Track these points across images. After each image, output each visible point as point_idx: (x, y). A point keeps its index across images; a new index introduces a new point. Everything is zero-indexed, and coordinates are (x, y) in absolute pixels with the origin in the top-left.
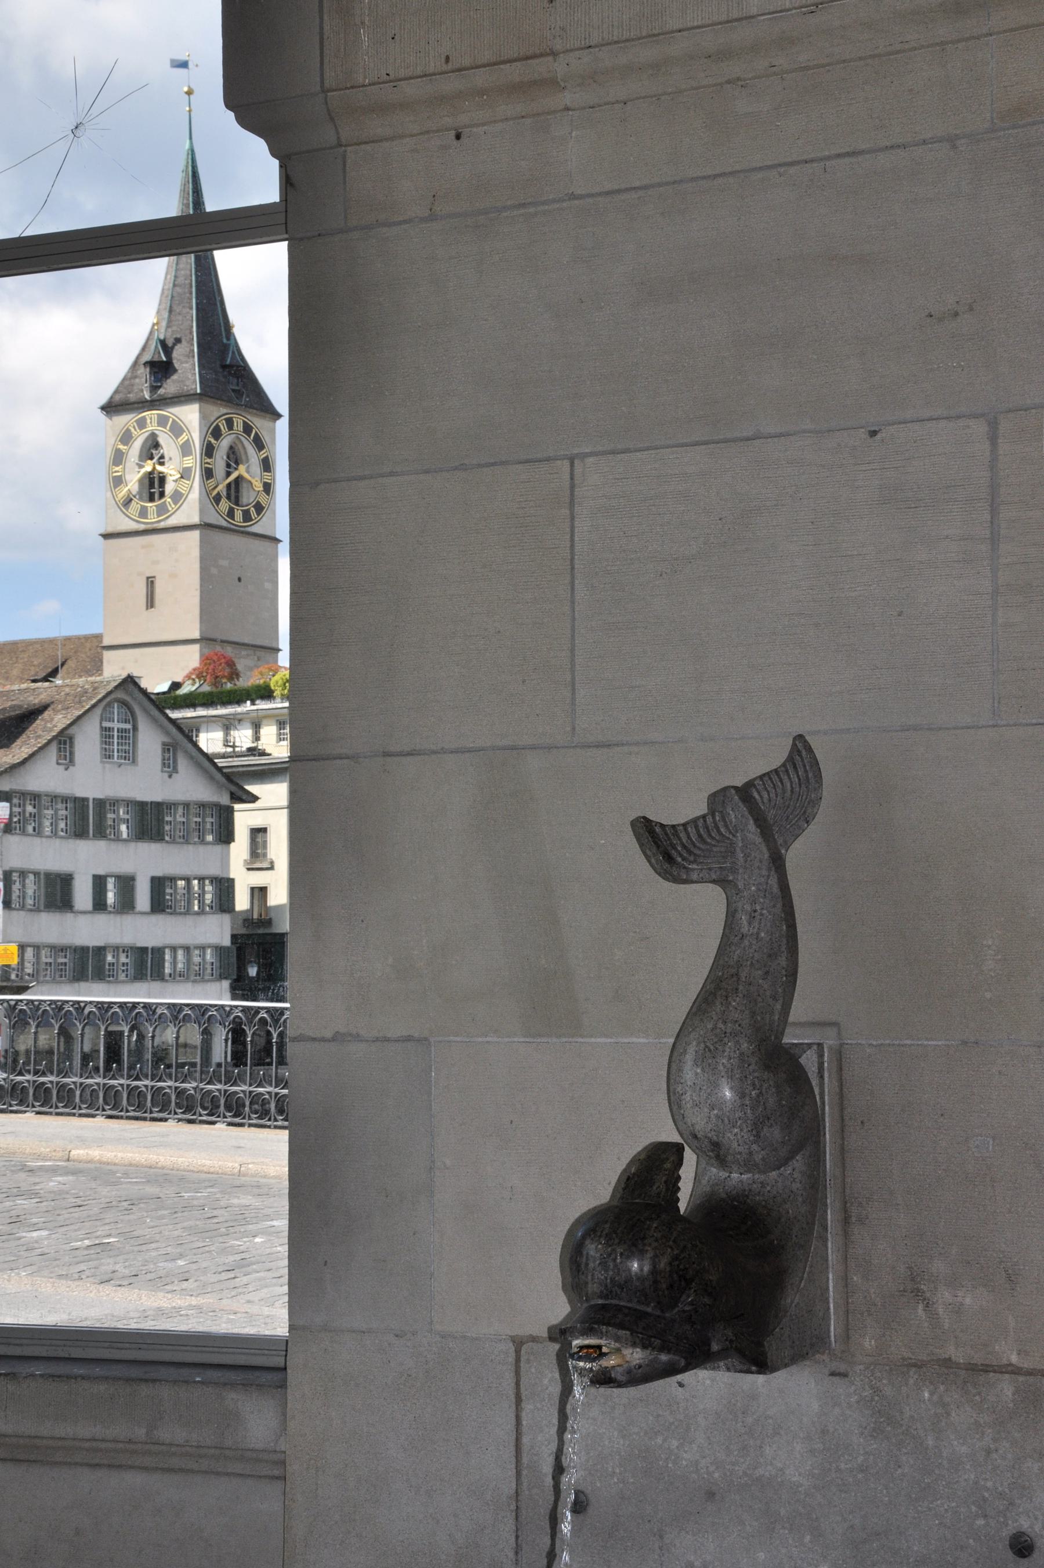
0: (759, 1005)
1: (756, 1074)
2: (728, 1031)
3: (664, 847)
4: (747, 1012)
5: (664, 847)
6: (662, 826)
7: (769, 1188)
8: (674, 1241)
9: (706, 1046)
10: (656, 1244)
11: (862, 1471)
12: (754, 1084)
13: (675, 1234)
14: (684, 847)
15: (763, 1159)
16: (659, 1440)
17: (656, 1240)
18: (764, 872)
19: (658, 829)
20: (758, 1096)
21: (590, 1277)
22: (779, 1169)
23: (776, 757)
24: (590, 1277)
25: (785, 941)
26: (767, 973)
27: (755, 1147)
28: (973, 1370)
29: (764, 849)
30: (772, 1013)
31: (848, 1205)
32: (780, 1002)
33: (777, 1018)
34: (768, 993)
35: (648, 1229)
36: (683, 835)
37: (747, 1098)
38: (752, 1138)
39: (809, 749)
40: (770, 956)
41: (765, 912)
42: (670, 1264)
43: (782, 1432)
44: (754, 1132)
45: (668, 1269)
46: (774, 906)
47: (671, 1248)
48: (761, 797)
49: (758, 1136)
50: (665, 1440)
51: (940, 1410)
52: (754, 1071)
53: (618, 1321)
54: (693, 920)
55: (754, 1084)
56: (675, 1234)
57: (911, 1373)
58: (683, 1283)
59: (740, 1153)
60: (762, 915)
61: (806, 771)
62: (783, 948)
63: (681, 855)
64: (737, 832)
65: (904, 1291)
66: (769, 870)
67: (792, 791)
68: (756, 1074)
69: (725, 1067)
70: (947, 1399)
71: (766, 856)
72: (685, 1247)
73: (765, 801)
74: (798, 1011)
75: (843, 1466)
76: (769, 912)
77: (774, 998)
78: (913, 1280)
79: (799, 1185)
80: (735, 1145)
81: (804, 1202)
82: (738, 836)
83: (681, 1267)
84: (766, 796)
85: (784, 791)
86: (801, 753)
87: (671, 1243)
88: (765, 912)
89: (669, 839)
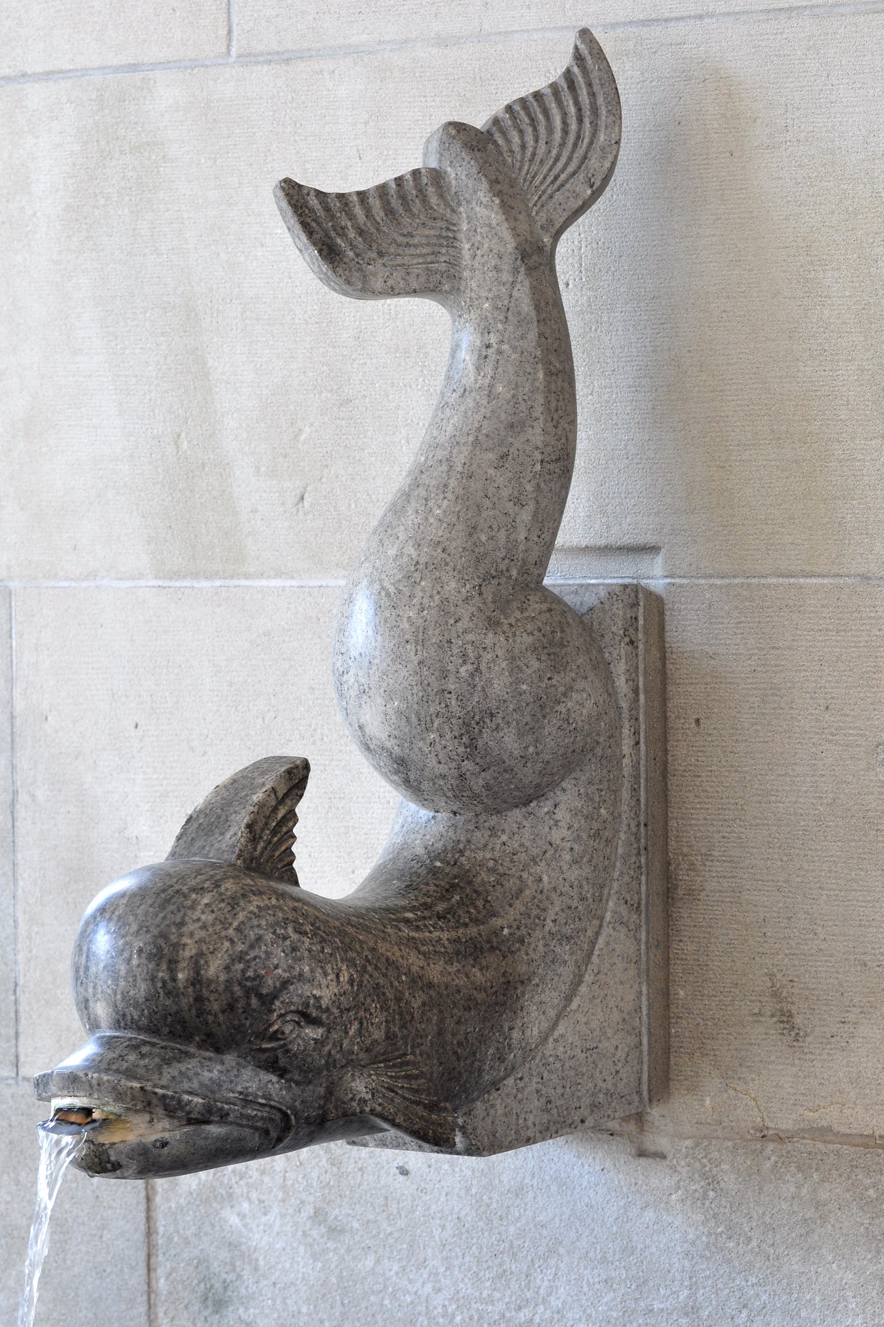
0: (484, 514)
1: (470, 637)
2: (423, 560)
3: (346, 235)
4: (460, 527)
5: (346, 235)
6: (319, 193)
7: (504, 838)
8: (238, 930)
9: (383, 588)
10: (203, 934)
11: (687, 1314)
12: (464, 655)
13: (241, 916)
14: (361, 232)
15: (487, 787)
16: (370, 1262)
17: (204, 927)
18: (506, 277)
19: (313, 202)
20: (472, 675)
21: (90, 990)
22: (526, 804)
23: (563, 61)
24: (90, 990)
25: (540, 399)
26: (504, 457)
27: (468, 765)
28: (866, 1146)
29: (507, 235)
30: (513, 527)
31: (672, 868)
32: (531, 506)
33: (522, 537)
34: (505, 493)
35: (192, 908)
36: (358, 210)
37: (452, 678)
38: (461, 749)
39: (599, 55)
40: (512, 426)
41: (505, 347)
42: (227, 968)
43: (562, 1250)
44: (465, 739)
45: (223, 977)
46: (523, 337)
47: (232, 941)
48: (508, 141)
49: (472, 745)
50: (378, 1261)
51: (810, 1213)
52: (465, 632)
53: (125, 1065)
54: (414, 361)
55: (464, 655)
56: (241, 916)
57: (768, 1151)
58: (254, 1002)
59: (443, 777)
60: (500, 352)
61: (592, 95)
62: (538, 411)
63: (353, 247)
64: (459, 204)
65: (760, 1014)
66: (515, 271)
67: (565, 131)
68: (470, 637)
69: (412, 624)
70: (824, 1196)
71: (511, 245)
72: (259, 939)
73: (516, 148)
74: (576, 524)
75: (657, 1306)
76: (514, 348)
77: (519, 502)
78: (775, 995)
79: (565, 832)
80: (432, 762)
81: (575, 862)
82: (480, 211)
83: (250, 974)
84: (516, 140)
85: (550, 130)
86: (589, 56)
87: (231, 932)
88: (505, 347)
89: (333, 217)
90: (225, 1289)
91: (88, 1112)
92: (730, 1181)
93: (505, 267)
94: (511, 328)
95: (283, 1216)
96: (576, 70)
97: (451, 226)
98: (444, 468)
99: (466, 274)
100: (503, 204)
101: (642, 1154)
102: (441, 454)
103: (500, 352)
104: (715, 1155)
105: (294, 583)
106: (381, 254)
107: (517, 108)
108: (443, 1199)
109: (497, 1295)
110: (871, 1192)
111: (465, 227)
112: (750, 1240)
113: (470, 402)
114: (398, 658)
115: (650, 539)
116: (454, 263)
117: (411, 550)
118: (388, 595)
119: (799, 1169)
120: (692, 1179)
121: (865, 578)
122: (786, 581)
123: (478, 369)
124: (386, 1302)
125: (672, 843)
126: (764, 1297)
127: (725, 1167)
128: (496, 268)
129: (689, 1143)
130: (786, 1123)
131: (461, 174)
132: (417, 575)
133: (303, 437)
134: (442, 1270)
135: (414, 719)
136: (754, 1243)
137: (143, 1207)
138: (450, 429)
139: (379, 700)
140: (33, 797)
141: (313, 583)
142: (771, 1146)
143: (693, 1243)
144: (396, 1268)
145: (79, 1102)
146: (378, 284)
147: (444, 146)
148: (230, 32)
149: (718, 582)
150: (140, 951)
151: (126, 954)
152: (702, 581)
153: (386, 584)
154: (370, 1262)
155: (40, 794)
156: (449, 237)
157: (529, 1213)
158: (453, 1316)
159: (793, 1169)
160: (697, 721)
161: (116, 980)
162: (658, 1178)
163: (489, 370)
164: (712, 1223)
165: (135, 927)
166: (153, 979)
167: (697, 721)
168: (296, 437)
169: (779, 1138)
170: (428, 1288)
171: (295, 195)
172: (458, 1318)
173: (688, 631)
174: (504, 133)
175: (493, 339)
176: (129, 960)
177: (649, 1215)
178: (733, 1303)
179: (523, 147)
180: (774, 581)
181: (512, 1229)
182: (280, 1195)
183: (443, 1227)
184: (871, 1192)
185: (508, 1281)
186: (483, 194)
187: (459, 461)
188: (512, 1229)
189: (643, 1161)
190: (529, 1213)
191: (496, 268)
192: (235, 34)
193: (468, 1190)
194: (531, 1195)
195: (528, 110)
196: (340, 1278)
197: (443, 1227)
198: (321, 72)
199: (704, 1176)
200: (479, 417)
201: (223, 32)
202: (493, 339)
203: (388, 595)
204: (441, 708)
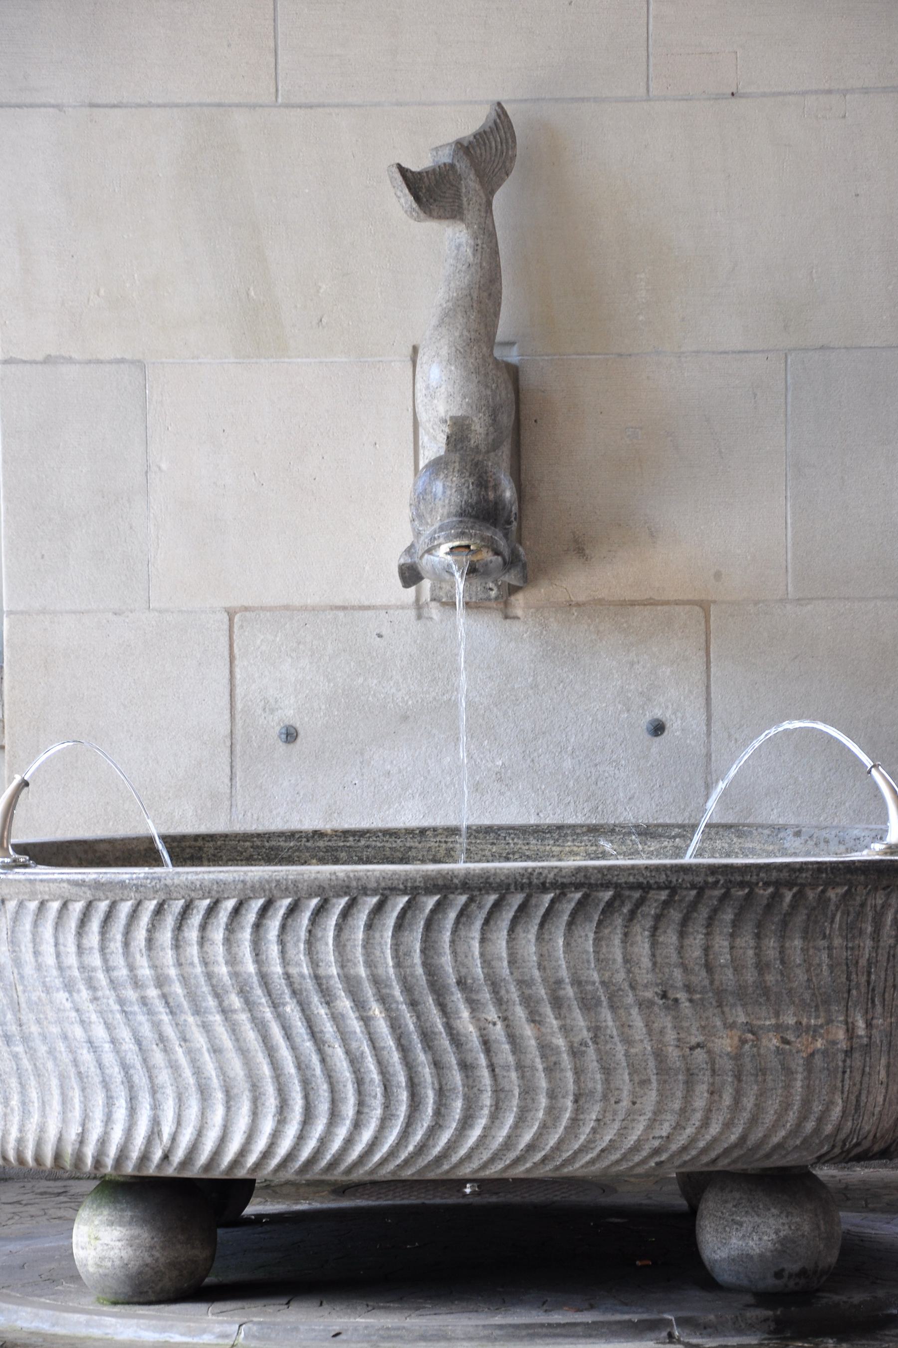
5: (430, 191)
16: (361, 680)
50: (365, 680)
65: (568, 550)
88: (485, 246)
90: (276, 702)
91: (468, 547)
92: (554, 626)
93: (483, 210)
94: (486, 237)
95: (311, 663)
96: (498, 121)
97: (458, 190)
98: (469, 298)
99: (465, 212)
100: (480, 182)
101: (506, 617)
102: (465, 292)
103: (482, 248)
104: (547, 614)
105: (317, 360)
106: (435, 200)
107: (478, 137)
108: (401, 647)
109: (431, 689)
110: (625, 625)
111: (464, 190)
112: (564, 652)
113: (473, 269)
114: (468, 380)
115: (512, 339)
116: (460, 207)
117: (465, 333)
118: (460, 352)
119: (589, 617)
120: (534, 626)
121: (620, 355)
122: (581, 357)
123: (474, 255)
124: (370, 699)
125: (523, 476)
126: (571, 677)
127: (552, 620)
128: (479, 210)
129: (532, 610)
130: (582, 598)
131: (462, 166)
132: (472, 344)
133: (322, 291)
134: (401, 681)
135: (474, 407)
136: (567, 653)
137: (228, 666)
138: (466, 282)
139: (459, 399)
140: (160, 468)
141: (327, 360)
142: (574, 609)
143: (535, 656)
144: (375, 681)
145: (464, 542)
146: (435, 214)
147: (456, 153)
148: (277, 90)
149: (546, 358)
150: (473, 483)
151: (466, 485)
152: (538, 358)
153: (458, 347)
154: (361, 680)
155: (164, 466)
156: (458, 196)
157: (448, 649)
158: (407, 701)
159: (586, 617)
160: (536, 421)
161: (462, 495)
162: (516, 627)
163: (479, 255)
164: (545, 646)
165: (467, 474)
166: (479, 495)
167: (536, 421)
168: (318, 291)
169: (578, 605)
170: (394, 690)
171: (403, 171)
172: (410, 703)
173: (530, 378)
174: (473, 148)
175: (479, 242)
176: (468, 487)
177: (512, 645)
178: (555, 681)
179: (481, 155)
180: (574, 357)
181: (439, 658)
182: (309, 653)
183: (402, 660)
184: (625, 625)
185: (437, 683)
186: (472, 176)
187: (475, 296)
188: (439, 658)
189: (508, 620)
190: (448, 649)
191: (479, 210)
192: (280, 92)
193: (415, 642)
194: (449, 642)
195: (481, 137)
196: (344, 690)
197: (402, 660)
198: (330, 114)
199: (541, 625)
200: (478, 276)
201: (273, 90)
202: (479, 242)
203: (460, 352)
204: (485, 402)
